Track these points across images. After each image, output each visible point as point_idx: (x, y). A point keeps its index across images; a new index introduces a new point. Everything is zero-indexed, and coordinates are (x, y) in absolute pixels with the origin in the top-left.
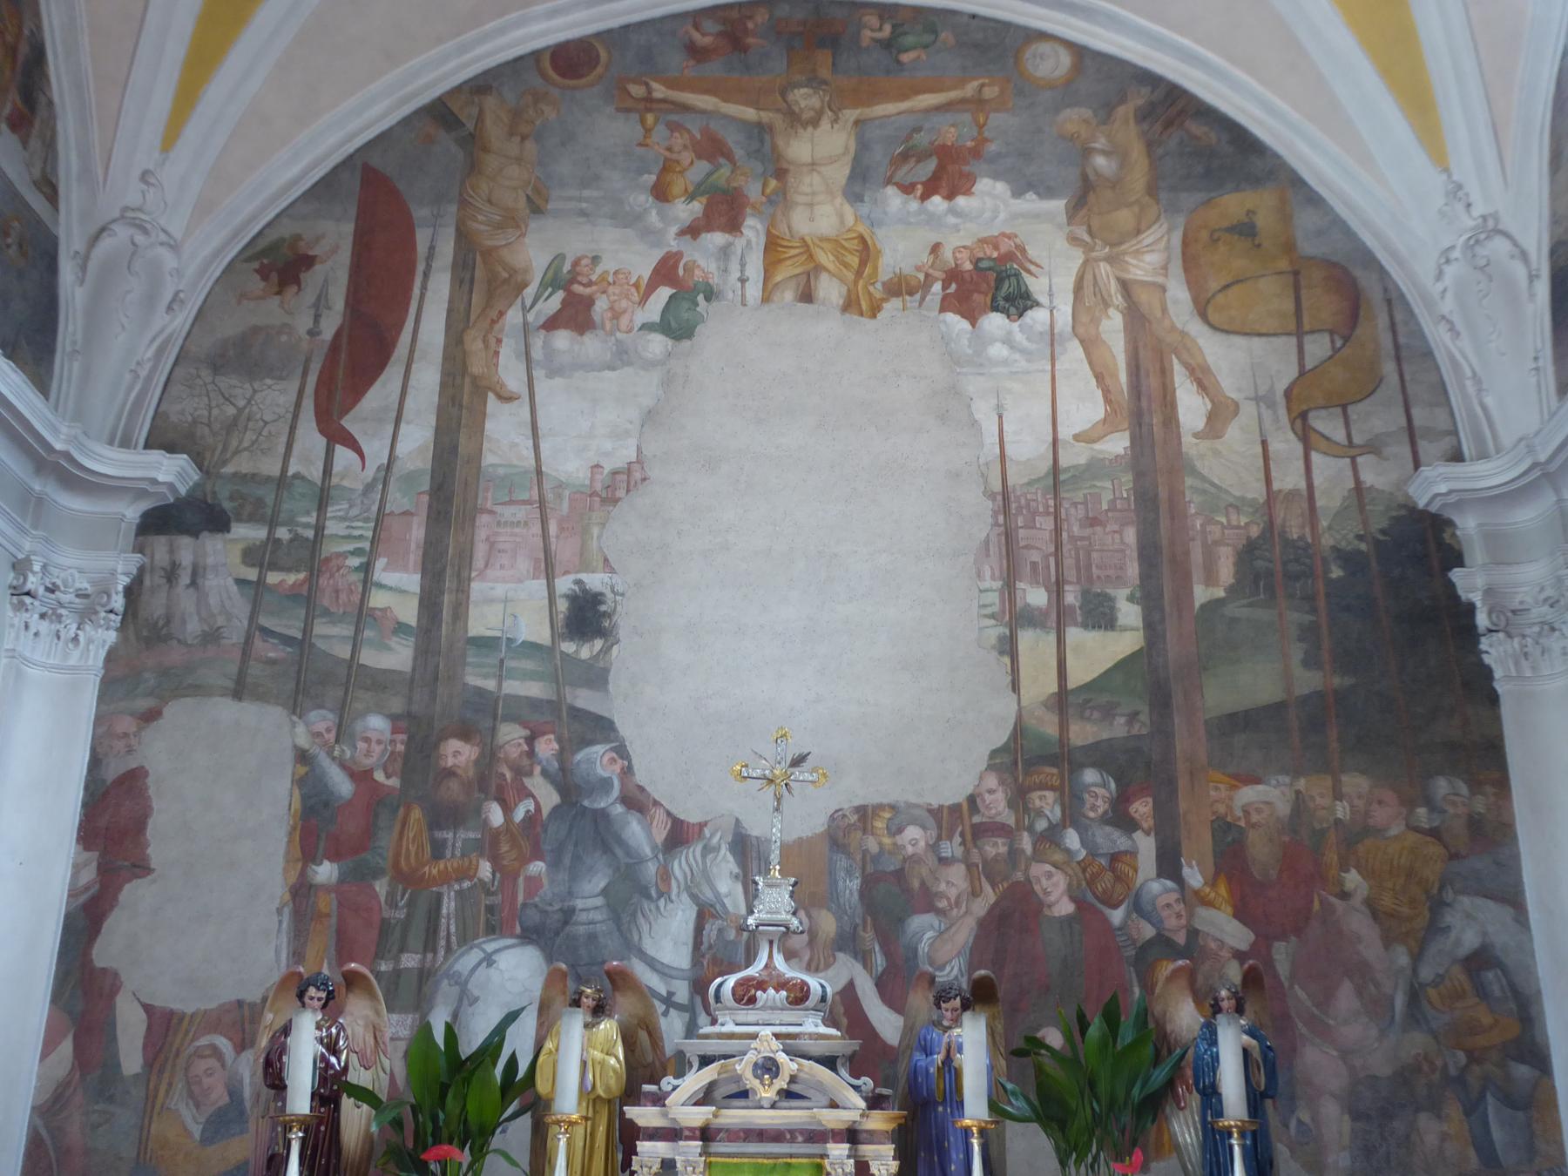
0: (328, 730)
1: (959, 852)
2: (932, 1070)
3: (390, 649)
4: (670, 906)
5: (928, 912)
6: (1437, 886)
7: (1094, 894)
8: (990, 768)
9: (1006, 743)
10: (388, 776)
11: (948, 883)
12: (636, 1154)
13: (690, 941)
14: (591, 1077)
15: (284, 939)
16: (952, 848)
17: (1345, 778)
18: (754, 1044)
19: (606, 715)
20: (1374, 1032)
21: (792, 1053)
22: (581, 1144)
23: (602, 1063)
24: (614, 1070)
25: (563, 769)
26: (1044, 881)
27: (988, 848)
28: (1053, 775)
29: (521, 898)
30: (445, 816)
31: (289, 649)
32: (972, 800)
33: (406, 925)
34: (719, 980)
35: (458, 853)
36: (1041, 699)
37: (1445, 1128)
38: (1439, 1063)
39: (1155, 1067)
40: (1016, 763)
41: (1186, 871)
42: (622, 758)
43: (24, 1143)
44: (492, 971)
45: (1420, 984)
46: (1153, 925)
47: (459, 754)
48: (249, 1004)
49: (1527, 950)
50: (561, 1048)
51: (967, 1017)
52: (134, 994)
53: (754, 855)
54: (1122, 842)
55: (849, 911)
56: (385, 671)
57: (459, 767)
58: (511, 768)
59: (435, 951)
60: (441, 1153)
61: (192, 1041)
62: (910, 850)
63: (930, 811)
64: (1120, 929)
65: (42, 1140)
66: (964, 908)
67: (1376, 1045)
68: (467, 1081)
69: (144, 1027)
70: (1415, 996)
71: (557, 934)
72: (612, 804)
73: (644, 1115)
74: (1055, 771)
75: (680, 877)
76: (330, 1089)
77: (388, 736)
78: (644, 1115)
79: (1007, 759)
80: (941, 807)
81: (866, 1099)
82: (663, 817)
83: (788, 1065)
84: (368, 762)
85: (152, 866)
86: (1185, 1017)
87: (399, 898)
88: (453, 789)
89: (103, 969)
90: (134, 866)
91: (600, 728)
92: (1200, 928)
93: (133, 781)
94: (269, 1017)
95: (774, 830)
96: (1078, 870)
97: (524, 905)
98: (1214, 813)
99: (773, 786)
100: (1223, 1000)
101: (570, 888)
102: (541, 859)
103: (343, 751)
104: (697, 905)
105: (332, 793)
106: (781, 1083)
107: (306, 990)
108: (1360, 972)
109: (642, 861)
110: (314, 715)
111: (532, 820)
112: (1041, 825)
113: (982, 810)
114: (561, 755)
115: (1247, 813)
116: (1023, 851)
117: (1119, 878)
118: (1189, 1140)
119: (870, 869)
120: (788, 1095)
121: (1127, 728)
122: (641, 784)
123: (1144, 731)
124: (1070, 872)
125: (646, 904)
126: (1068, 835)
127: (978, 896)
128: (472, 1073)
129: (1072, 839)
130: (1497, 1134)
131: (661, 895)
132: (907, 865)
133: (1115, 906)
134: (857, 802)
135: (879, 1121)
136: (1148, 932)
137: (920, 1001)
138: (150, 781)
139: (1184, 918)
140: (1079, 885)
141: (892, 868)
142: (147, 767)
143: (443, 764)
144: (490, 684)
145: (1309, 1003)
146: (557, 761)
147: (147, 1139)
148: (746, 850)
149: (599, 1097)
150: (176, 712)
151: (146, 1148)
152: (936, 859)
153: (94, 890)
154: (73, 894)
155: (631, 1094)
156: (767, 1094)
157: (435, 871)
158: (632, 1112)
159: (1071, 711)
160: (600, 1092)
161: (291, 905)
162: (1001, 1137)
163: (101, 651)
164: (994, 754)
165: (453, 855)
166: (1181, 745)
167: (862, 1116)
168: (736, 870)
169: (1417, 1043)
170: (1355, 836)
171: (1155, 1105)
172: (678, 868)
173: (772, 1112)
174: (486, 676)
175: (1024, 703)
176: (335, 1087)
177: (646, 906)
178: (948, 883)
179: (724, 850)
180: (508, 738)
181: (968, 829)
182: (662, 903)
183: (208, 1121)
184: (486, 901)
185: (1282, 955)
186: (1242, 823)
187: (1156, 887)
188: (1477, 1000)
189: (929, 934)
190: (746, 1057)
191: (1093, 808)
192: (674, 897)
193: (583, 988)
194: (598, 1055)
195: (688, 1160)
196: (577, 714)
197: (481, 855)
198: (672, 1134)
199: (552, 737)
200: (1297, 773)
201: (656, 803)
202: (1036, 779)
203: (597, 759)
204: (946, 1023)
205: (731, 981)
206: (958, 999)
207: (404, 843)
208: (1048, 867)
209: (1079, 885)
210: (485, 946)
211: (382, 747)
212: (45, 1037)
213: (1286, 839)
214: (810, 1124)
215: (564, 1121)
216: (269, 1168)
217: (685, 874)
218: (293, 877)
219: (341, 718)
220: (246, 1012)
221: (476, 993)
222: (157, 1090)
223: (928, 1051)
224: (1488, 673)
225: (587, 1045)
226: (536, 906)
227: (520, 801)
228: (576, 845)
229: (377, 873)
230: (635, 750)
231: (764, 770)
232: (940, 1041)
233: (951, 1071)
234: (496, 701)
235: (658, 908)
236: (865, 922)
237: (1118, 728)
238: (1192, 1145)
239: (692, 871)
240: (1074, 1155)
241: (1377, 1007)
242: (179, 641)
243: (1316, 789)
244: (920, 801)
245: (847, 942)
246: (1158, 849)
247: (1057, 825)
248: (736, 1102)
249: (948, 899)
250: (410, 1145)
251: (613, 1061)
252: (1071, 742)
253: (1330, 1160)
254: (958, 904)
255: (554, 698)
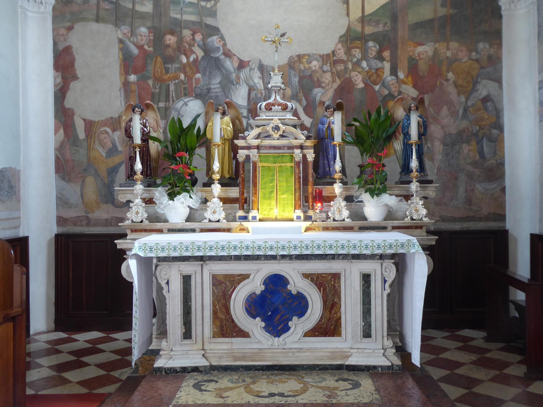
0: (128, 32)
1: (329, 68)
2: (324, 129)
3: (145, 5)
4: (240, 87)
5: (320, 87)
6: (476, 77)
7: (370, 81)
8: (339, 42)
9: (344, 34)
10: (149, 47)
11: (325, 78)
12: (238, 154)
13: (247, 98)
14: (223, 133)
15: (122, 99)
16: (326, 68)
17: (451, 43)
18: (272, 121)
19: (217, 26)
20: (452, 121)
21: (284, 124)
22: (221, 152)
23: (226, 129)
24: (230, 131)
25: (204, 44)
26: (355, 78)
27: (338, 67)
28: (359, 44)
29: (194, 85)
30: (168, 60)
31: (112, 5)
32: (333, 52)
33: (159, 94)
34: (260, 104)
35: (173, 71)
36: (357, 18)
37: (470, 148)
38: (471, 129)
39: (390, 128)
40: (347, 40)
41: (399, 74)
42: (223, 40)
43: (54, 158)
44: (187, 107)
45: (468, 107)
46: (388, 90)
47: (171, 40)
48: (115, 118)
49: (501, 96)
50: (214, 125)
51: (336, 112)
52: (79, 116)
53: (266, 71)
54: (379, 65)
55: (295, 88)
56: (144, 13)
57: (171, 44)
58: (188, 44)
59: (169, 102)
60: (181, 154)
61: (99, 129)
62: (314, 68)
63: (320, 56)
64: (378, 91)
65: (59, 157)
66: (330, 86)
67: (452, 125)
68: (186, 135)
69: (84, 125)
70: (465, 110)
71: (206, 96)
72: (221, 55)
73: (239, 143)
74: (359, 42)
75: (243, 78)
76: (146, 137)
77: (147, 34)
78: (239, 143)
79: (345, 39)
80: (324, 55)
81: (305, 137)
82: (237, 59)
83: (282, 127)
84: (142, 43)
85: (79, 76)
86: (400, 113)
87: (156, 86)
88: (170, 51)
89: (69, 108)
90: (73, 77)
91: (215, 31)
92: (402, 91)
93: (68, 50)
94: (124, 117)
95: (276, 58)
96: (366, 74)
97: (195, 87)
98: (409, 55)
99: (275, 44)
100: (412, 107)
101: (209, 82)
102: (200, 73)
103: (134, 39)
104: (249, 86)
105: (132, 53)
106: (280, 133)
107: (135, 109)
108: (450, 104)
109: (231, 73)
110: (123, 27)
111: (195, 60)
112: (355, 60)
113: (336, 55)
114: (204, 40)
115: (419, 55)
116: (349, 68)
117: (378, 76)
118: (399, 148)
119: (301, 74)
120: (282, 136)
121: (383, 28)
122: (229, 49)
123: (389, 29)
124: (363, 74)
125: (233, 87)
126: (363, 63)
127: (335, 82)
128: (188, 132)
129: (364, 64)
130: (486, 149)
131: (237, 83)
132: (313, 73)
133: (377, 85)
134: (298, 54)
135: (309, 143)
136: (386, 92)
137: (320, 111)
138: (74, 50)
139: (397, 88)
140: (366, 78)
141: (308, 74)
142: (72, 45)
143: (166, 43)
144: (178, 16)
145: (433, 113)
146: (202, 42)
147: (90, 157)
148: (262, 68)
149: (225, 138)
150: (78, 27)
151: (90, 159)
152: (322, 71)
153: (62, 84)
154: (55, 86)
155: (236, 136)
156: (276, 136)
157: (167, 77)
158: (236, 142)
159: (366, 22)
160: (226, 137)
161: (123, 88)
162: (344, 149)
163: (50, 6)
164: (341, 37)
165: (172, 72)
166: (400, 33)
167: (304, 141)
168: (260, 75)
169: (464, 124)
170: (452, 61)
171: (389, 138)
172: (242, 75)
173: (278, 141)
174: (177, 14)
175: (350, 20)
176: (147, 137)
177: (233, 87)
178: (325, 78)
179: (256, 69)
180: (186, 34)
181: (332, 61)
182: (238, 86)
183: (107, 152)
184: (183, 86)
185: (426, 98)
186: (417, 58)
187: (389, 78)
188: (484, 111)
189: (320, 94)
190: (270, 126)
191: (371, 54)
192: (241, 84)
193: (219, 107)
194: (225, 127)
195: (254, 155)
196: (208, 26)
197: (181, 72)
198: (249, 148)
199: (200, 34)
200: (436, 41)
201: (234, 55)
202: (354, 45)
203: (214, 41)
204: (328, 116)
205: (264, 104)
206: (332, 108)
207: (156, 69)
208: (356, 73)
209: (366, 78)
210: (184, 100)
211: (146, 37)
212: (55, 129)
213: (431, 63)
214: (289, 144)
215: (217, 145)
216: (130, 160)
217: (244, 76)
218: (123, 80)
219: (132, 28)
220: (114, 121)
221: (183, 114)
222: (91, 143)
223: (323, 124)
224: (499, 8)
225: (222, 124)
226: (199, 88)
227: (192, 55)
228: (210, 68)
229: (149, 78)
230: (227, 38)
231: (272, 38)
232: (327, 121)
233: (330, 129)
234: (181, 22)
235: (236, 87)
236: (300, 90)
237: (380, 28)
238: (400, 150)
239: (246, 76)
240: (365, 153)
241: (454, 114)
242: (75, 3)
243: (441, 47)
244: (318, 53)
245: (294, 97)
246: (391, 67)
247: (360, 60)
248: (267, 139)
249: (325, 83)
250: (171, 153)
251: (229, 128)
252: (365, 33)
253: (436, 157)
254: (328, 85)
255: (200, 21)
